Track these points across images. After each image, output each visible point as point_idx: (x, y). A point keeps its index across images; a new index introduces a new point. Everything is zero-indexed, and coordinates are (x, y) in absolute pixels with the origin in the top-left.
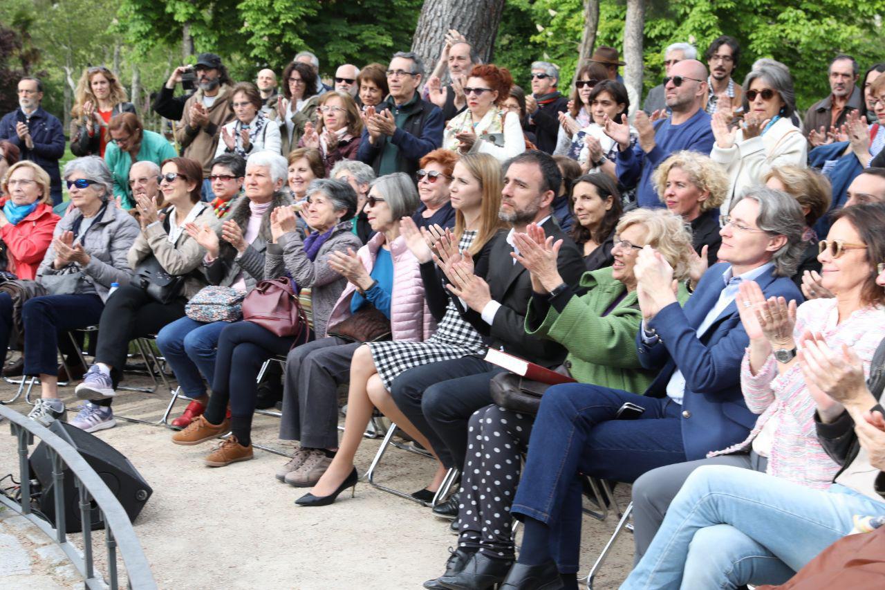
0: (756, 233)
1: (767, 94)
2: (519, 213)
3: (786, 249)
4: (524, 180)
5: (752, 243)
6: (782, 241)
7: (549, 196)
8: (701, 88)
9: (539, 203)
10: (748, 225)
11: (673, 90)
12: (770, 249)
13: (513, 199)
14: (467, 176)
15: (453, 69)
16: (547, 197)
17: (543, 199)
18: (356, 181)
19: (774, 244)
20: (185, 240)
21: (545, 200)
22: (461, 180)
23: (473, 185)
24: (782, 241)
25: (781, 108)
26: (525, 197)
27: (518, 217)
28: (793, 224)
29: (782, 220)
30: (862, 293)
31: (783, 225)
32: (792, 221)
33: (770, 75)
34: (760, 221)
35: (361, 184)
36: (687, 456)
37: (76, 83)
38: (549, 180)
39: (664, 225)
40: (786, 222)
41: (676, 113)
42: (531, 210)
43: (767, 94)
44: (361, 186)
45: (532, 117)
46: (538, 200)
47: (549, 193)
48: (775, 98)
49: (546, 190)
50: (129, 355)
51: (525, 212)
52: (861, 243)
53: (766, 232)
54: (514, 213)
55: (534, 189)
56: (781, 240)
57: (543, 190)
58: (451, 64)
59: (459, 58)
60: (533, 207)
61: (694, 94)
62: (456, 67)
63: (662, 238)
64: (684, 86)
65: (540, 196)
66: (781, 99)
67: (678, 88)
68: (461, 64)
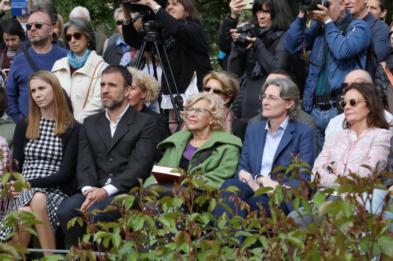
0: (281, 101)
1: (77, 36)
3: (294, 107)
5: (279, 106)
6: (293, 103)
8: (51, 30)
9: (124, 95)
10: (276, 97)
11: (35, 32)
12: (288, 107)
13: (110, 94)
20: (22, 234)
24: (293, 103)
25: (88, 42)
26: (116, 93)
27: (114, 104)
29: (291, 92)
33: (77, 24)
34: (281, 94)
37: (245, 205)
38: (127, 80)
40: (293, 93)
41: (39, 47)
43: (77, 36)
48: (83, 37)
51: (118, 100)
52: (363, 99)
53: (285, 99)
54: (112, 102)
61: (48, 34)
63: (217, 106)
64: (44, 27)
65: (125, 89)
66: (87, 37)
67: (39, 30)
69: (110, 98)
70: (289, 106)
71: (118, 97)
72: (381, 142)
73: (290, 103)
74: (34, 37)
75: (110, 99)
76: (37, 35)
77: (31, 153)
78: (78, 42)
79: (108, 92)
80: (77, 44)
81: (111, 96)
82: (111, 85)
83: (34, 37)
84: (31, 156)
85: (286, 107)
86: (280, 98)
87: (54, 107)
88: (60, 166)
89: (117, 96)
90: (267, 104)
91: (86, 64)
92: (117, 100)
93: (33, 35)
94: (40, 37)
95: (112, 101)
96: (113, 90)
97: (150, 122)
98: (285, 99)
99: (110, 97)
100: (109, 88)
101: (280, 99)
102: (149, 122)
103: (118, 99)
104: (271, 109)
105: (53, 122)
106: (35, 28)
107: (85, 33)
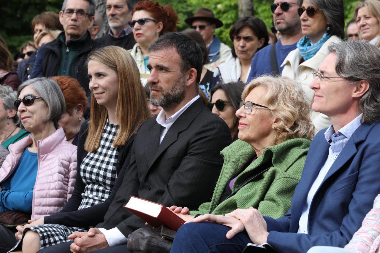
0: (339, 82)
2: (167, 96)
4: (166, 65)
5: (337, 91)
7: (193, 74)
9: (184, 82)
11: (280, 17)
12: (355, 95)
13: (159, 84)
14: (102, 69)
15: (110, 17)
16: (192, 75)
17: (188, 77)
18: (4, 104)
19: (358, 90)
21: (190, 78)
22: (99, 75)
23: (111, 75)
24: (365, 86)
26: (168, 81)
28: (372, 69)
29: (359, 66)
30: (361, 121)
31: (361, 70)
32: (371, 66)
34: (339, 68)
35: (9, 108)
36: (109, 161)
39: (283, 86)
42: (177, 91)
44: (8, 111)
45: (80, 118)
46: (182, 80)
47: (192, 71)
48: (318, 16)
49: (188, 69)
50: (208, 46)
51: (173, 94)
54: (162, 97)
55: (176, 70)
56: (363, 85)
57: (185, 69)
58: (109, 12)
59: (116, 7)
60: (178, 87)
62: (113, 15)
65: (184, 75)
67: (285, 14)
68: (118, 12)
69: (158, 91)
70: (358, 92)
71: (173, 88)
72: (348, 186)
73: (361, 87)
74: (278, 23)
75: (160, 93)
76: (282, 21)
77: (103, 172)
78: (310, 21)
79: (156, 81)
80: (308, 23)
81: (161, 88)
82: (160, 68)
83: (278, 23)
84: (109, 179)
85: (351, 94)
86: (337, 75)
87: (50, 101)
88: (110, 193)
89: (171, 87)
90: (315, 86)
91: (318, 53)
92: (170, 92)
93: (278, 21)
94: (287, 23)
95: (163, 95)
96: (163, 77)
97: (208, 128)
98: (346, 79)
99: (159, 90)
100: (158, 75)
101: (336, 79)
102: (205, 129)
103: (172, 91)
104: (323, 95)
105: (117, 127)
106: (281, 12)
107: (324, 10)
